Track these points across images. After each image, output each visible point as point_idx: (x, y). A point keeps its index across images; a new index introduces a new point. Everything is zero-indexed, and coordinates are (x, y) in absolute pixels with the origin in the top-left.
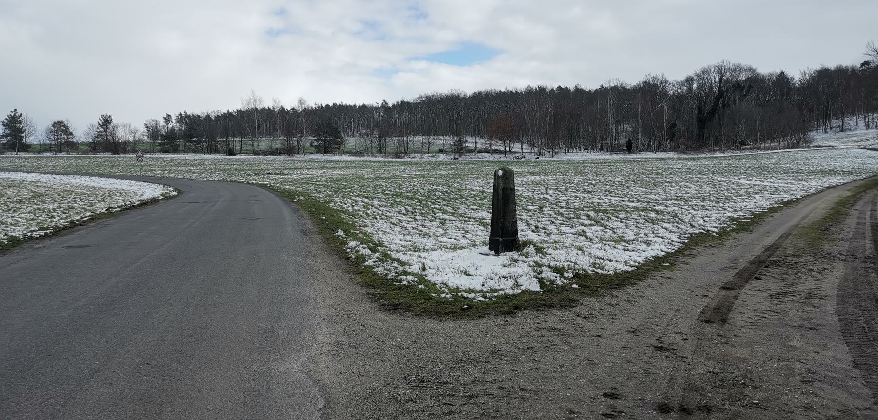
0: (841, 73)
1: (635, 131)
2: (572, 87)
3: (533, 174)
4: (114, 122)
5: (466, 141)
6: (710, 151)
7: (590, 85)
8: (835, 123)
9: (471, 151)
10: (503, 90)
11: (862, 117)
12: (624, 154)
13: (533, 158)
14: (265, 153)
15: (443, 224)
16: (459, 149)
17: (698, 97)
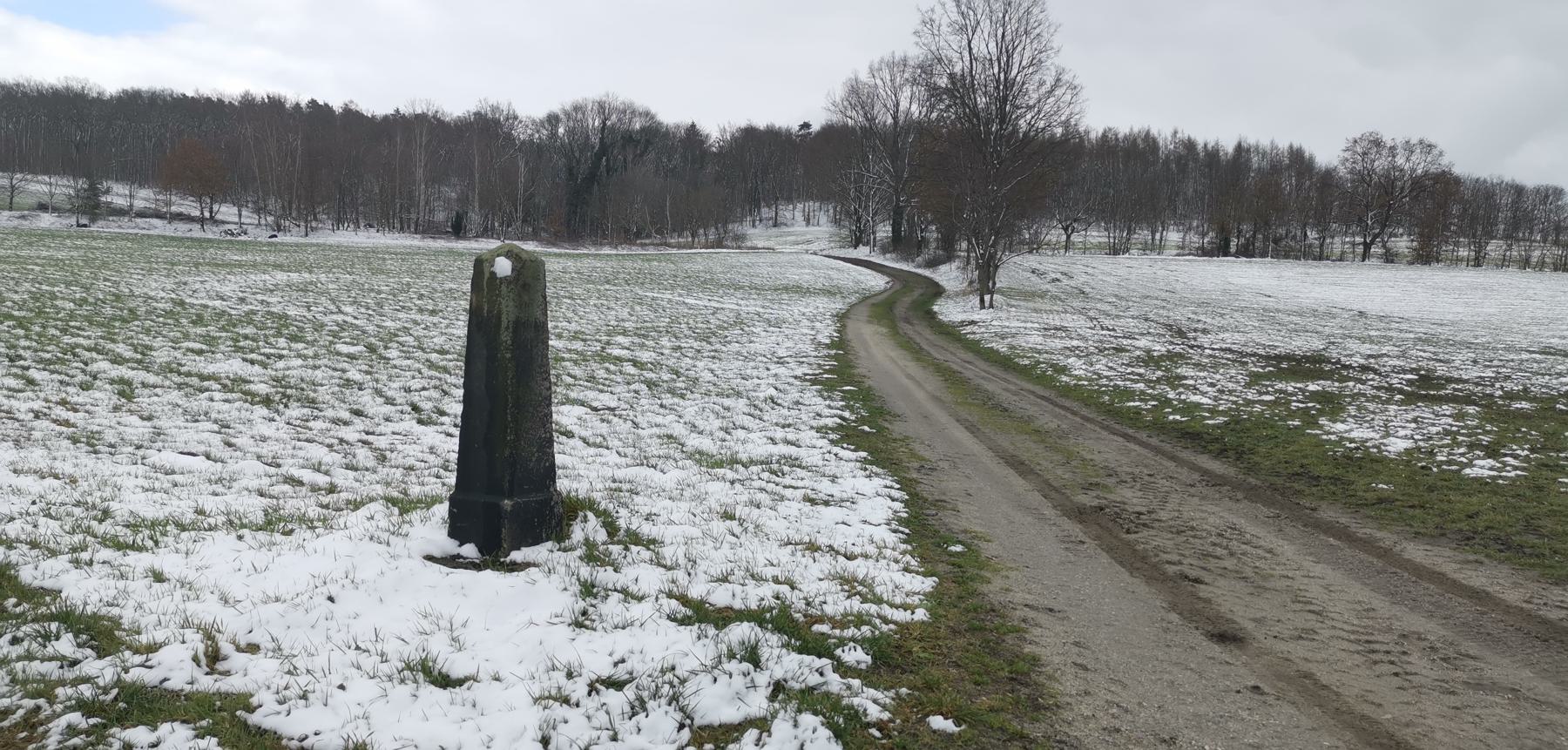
0: (773, 137)
1: (464, 200)
2: (337, 105)
3: (279, 267)
5: (107, 192)
6: (595, 244)
7: (375, 105)
8: (766, 212)
9: (120, 212)
10: (190, 94)
11: (800, 206)
12: (448, 240)
13: (263, 236)
15: (130, 398)
16: (91, 207)
17: (567, 151)
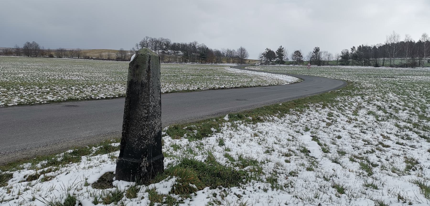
4: (320, 51)
14: (397, 66)
